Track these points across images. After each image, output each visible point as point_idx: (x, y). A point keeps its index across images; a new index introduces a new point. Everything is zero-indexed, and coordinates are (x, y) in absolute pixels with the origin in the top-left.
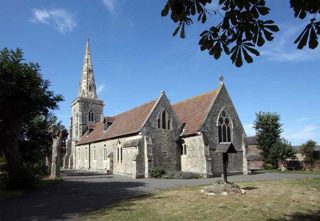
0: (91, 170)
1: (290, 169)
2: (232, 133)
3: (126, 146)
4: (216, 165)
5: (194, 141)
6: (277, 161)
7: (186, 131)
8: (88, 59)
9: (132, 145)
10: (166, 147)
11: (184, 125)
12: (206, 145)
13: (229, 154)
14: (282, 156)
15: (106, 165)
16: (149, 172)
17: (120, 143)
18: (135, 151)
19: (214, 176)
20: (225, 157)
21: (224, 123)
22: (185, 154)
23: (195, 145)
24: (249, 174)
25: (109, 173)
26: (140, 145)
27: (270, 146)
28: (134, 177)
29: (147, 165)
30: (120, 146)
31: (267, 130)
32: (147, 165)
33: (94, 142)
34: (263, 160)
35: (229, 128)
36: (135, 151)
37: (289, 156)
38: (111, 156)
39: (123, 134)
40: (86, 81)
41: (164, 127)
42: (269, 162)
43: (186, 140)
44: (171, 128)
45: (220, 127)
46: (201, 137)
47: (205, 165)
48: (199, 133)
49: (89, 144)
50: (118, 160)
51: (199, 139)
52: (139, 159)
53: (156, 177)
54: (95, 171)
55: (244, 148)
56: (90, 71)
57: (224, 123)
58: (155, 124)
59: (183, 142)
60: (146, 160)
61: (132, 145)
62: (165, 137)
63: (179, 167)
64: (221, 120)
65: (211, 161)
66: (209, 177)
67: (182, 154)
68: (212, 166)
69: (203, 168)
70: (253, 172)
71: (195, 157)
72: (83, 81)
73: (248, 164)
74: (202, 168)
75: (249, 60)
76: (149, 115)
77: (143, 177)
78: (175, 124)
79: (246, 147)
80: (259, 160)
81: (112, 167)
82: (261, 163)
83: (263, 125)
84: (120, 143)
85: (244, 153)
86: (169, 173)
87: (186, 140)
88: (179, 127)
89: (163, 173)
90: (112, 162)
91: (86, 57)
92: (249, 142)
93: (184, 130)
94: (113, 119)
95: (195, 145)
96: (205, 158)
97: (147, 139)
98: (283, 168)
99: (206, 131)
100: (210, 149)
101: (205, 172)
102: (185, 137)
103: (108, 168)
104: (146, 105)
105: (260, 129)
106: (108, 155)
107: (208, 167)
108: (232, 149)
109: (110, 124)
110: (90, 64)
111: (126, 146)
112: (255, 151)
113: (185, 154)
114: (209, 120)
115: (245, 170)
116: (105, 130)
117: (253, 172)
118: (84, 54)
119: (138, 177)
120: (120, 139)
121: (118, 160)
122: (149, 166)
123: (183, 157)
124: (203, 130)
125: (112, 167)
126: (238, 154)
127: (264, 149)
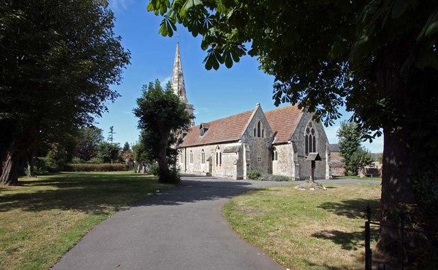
0: (187, 173)
1: (369, 176)
2: (317, 143)
3: (226, 151)
4: (302, 170)
5: (284, 148)
6: (357, 169)
7: (278, 140)
8: (178, 62)
9: (233, 150)
10: (261, 153)
11: (276, 133)
12: (295, 152)
13: (317, 162)
14: (361, 164)
15: (203, 168)
16: (247, 174)
17: (219, 148)
18: (236, 156)
19: (302, 179)
20: (313, 162)
21: (310, 133)
22: (276, 159)
23: (285, 152)
24: (330, 179)
25: (208, 175)
26: (240, 151)
27: (351, 153)
28: (235, 179)
29: (245, 169)
30: (219, 151)
31: (350, 139)
32: (245, 169)
33: (191, 147)
34: (345, 167)
35: (314, 137)
36: (236, 156)
37: (368, 164)
38: (210, 160)
39: (225, 141)
40: (177, 84)
41: (259, 136)
42: (350, 169)
43: (278, 148)
44: (265, 137)
45: (307, 136)
46: (291, 145)
47: (294, 170)
48: (289, 142)
49: (186, 148)
50: (217, 163)
51: (290, 146)
52: (239, 163)
53: (253, 179)
54: (192, 173)
55: (327, 155)
56: (180, 75)
57: (310, 133)
58: (251, 133)
59: (274, 149)
60: (245, 164)
61: (233, 150)
62: (261, 144)
63: (270, 171)
64: (308, 130)
65: (299, 168)
66: (297, 180)
67: (273, 159)
68: (300, 171)
69: (291, 173)
70: (334, 178)
71: (284, 163)
72: (174, 85)
73: (330, 170)
74: (291, 173)
75: (331, 125)
76: (247, 125)
77: (242, 178)
78: (269, 133)
79: (329, 155)
80: (341, 167)
81: (211, 170)
82: (342, 170)
83: (345, 134)
84: (219, 148)
85: (327, 160)
86: (264, 176)
87: (278, 148)
88: (271, 136)
89: (259, 175)
90: (211, 165)
91: (177, 61)
92: (332, 149)
93: (275, 138)
94: (208, 125)
95: (285, 152)
96: (293, 164)
97: (246, 146)
98: (361, 175)
99: (295, 140)
100: (298, 156)
101: (293, 175)
102: (276, 144)
103: (208, 171)
104: (242, 115)
105: (343, 138)
106: (206, 158)
107: (296, 172)
108: (318, 158)
109: (206, 130)
110: (180, 68)
111: (226, 151)
112: (338, 158)
113: (276, 159)
114: (298, 130)
115: (327, 175)
116: (202, 135)
117: (334, 178)
118: (174, 57)
119: (238, 179)
120: (219, 145)
121: (217, 163)
122: (248, 169)
123: (274, 162)
124: (292, 139)
125: (211, 170)
126: (322, 162)
127: (345, 157)
